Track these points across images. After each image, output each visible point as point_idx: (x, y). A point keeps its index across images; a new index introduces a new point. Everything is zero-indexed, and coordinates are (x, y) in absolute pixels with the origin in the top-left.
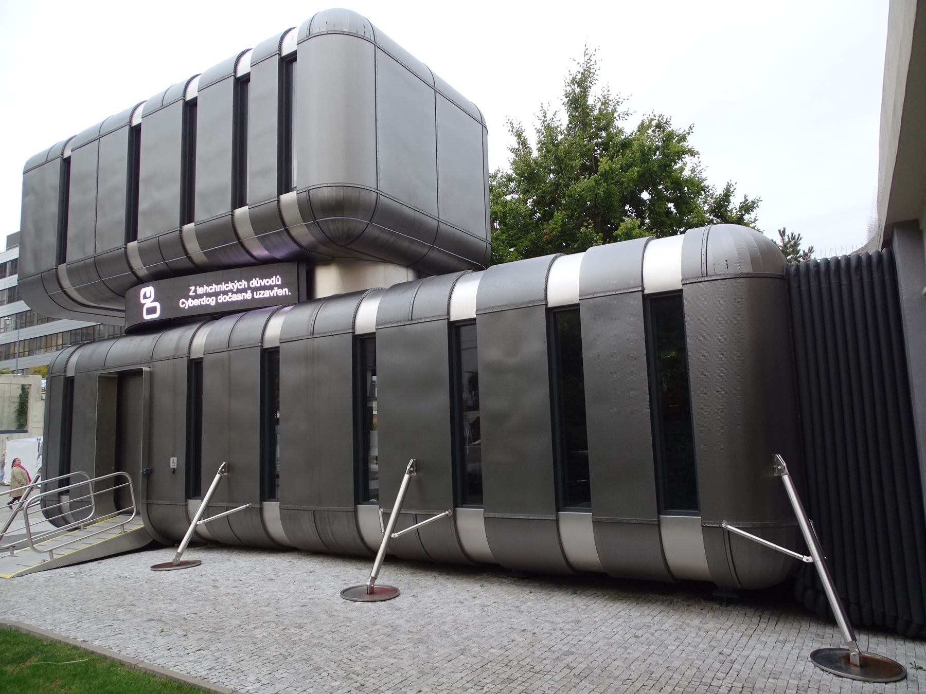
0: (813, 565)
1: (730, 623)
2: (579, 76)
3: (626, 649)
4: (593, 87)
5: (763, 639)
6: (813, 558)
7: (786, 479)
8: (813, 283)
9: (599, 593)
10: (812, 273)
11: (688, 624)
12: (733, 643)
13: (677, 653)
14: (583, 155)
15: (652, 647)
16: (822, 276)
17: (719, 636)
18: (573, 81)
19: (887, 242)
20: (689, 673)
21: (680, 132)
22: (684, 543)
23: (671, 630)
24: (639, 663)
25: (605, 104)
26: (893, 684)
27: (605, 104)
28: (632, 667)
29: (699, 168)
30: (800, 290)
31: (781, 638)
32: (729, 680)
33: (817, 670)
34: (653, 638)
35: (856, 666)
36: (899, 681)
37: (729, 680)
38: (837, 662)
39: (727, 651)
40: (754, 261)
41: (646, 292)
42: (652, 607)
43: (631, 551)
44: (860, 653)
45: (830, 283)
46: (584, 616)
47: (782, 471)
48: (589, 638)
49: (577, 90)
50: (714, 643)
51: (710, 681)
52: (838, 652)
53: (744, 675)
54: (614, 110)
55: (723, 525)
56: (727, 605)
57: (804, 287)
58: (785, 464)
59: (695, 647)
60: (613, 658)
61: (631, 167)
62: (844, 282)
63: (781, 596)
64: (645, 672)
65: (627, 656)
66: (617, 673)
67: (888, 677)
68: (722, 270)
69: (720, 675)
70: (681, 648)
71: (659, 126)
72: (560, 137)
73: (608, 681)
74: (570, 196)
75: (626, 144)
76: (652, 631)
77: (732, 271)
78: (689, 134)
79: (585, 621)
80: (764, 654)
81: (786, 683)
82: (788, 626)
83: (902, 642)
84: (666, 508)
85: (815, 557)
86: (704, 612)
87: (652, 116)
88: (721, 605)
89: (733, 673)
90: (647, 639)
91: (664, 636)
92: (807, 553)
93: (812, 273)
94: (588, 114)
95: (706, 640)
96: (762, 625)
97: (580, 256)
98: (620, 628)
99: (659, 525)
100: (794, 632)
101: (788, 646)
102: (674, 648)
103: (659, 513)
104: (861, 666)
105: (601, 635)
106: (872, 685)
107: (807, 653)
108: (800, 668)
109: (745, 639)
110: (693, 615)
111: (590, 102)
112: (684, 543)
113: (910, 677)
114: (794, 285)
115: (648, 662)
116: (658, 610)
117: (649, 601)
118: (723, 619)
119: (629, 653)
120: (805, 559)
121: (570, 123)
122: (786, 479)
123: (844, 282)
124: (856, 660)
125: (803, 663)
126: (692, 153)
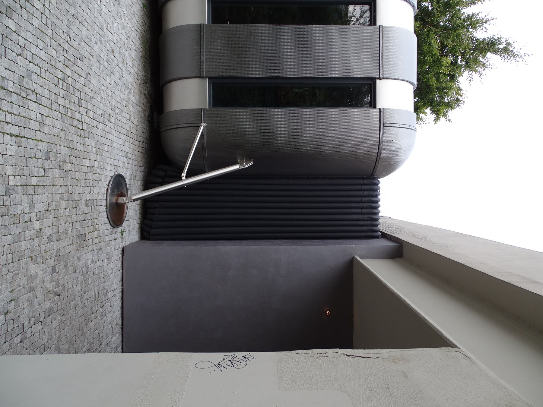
0: (180, 179)
1: (135, 122)
2: (511, 49)
3: (101, 41)
4: (500, 58)
5: (127, 144)
6: (184, 180)
7: (236, 167)
8: (365, 193)
9: (146, 27)
10: (372, 193)
11: (130, 93)
12: (120, 124)
13: (103, 82)
14: (454, 47)
15: (106, 63)
16: (369, 198)
17: (124, 114)
18: (509, 44)
19: (384, 236)
20: (88, 91)
21: (449, 114)
22: (188, 95)
23: (123, 79)
24: (89, 50)
25: (484, 65)
26: (108, 222)
27: (484, 65)
28: (83, 44)
29: (422, 123)
30: (361, 185)
31: (129, 155)
32: (88, 120)
33: (109, 178)
34: (114, 65)
35: (117, 200)
36: (111, 225)
37: (88, 120)
38: (117, 189)
39: (113, 120)
40: (388, 159)
41: (378, 81)
42: (140, 68)
43: (180, 55)
44: (125, 203)
45: (364, 202)
46: (125, 10)
47: (242, 164)
48: (104, 9)
49: (501, 46)
50: (117, 111)
51: (84, 106)
52: (125, 189)
53: (94, 130)
54: (476, 72)
55: (203, 124)
56: (148, 121)
57: (363, 187)
58: (246, 167)
59: (112, 96)
60: (89, 28)
61: (437, 81)
62: (364, 211)
63: (158, 158)
64: (81, 54)
65: (93, 41)
66: (74, 28)
67: (111, 219)
68: (386, 137)
69: (91, 114)
70: (109, 86)
71: (457, 100)
72: (471, 30)
73: (64, 18)
74: (428, 35)
75: (453, 78)
76: (120, 65)
77: (385, 145)
78: (446, 119)
79: (120, 10)
80: (115, 145)
81: (95, 159)
82: (139, 159)
83: (138, 222)
84: (213, 84)
85: (185, 181)
86: (142, 105)
87: (464, 96)
88: (148, 117)
89: (95, 123)
90: (113, 60)
91: (118, 75)
92: (187, 177)
93: (372, 193)
94: (482, 53)
95: (119, 105)
96: (137, 143)
97: (413, 31)
98: (118, 39)
99: (200, 77)
100: (135, 162)
101: (125, 160)
102: (108, 80)
103: (210, 78)
104: (117, 203)
105: (109, 21)
106: (105, 210)
107: (121, 171)
108: (109, 167)
109: (125, 132)
110: (138, 97)
111: (489, 55)
112: (188, 95)
113: (115, 230)
114: (366, 181)
115: (91, 58)
116: (138, 72)
117: (145, 66)
118: (138, 118)
119: (96, 43)
120: (184, 175)
121: (476, 40)
122: (236, 167)
123: (364, 211)
124: (121, 200)
125: (113, 169)
126: (436, 120)
